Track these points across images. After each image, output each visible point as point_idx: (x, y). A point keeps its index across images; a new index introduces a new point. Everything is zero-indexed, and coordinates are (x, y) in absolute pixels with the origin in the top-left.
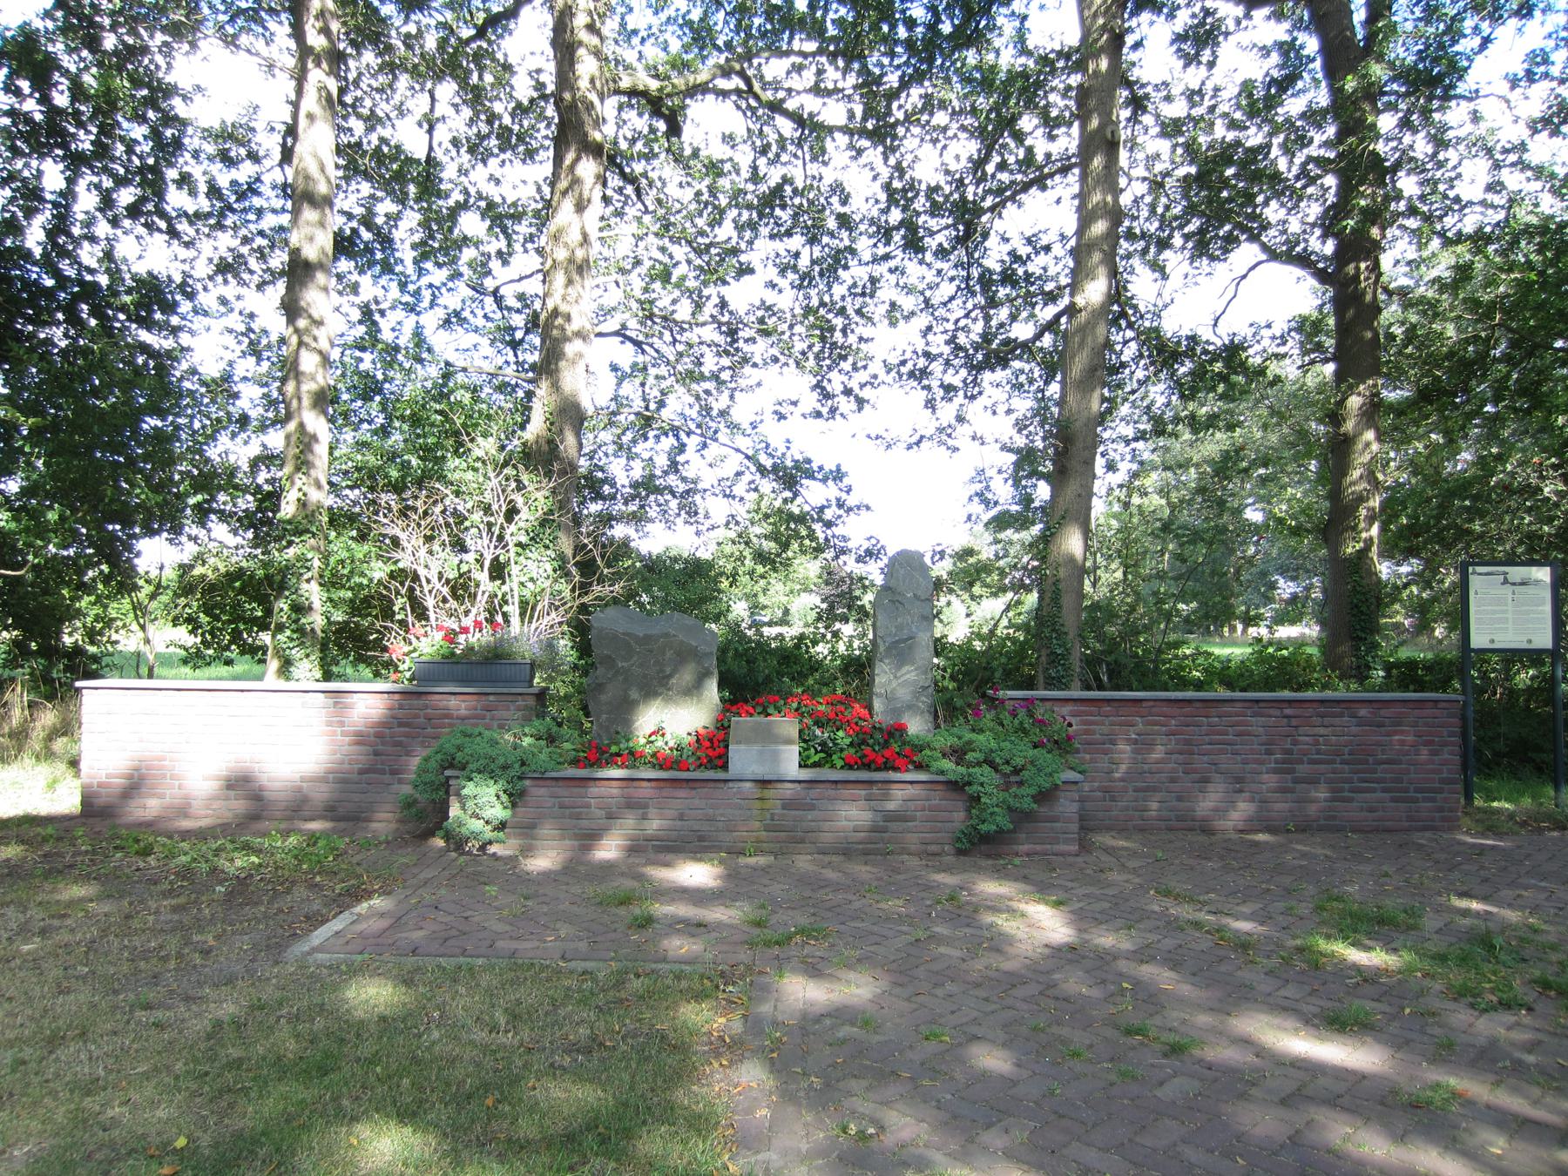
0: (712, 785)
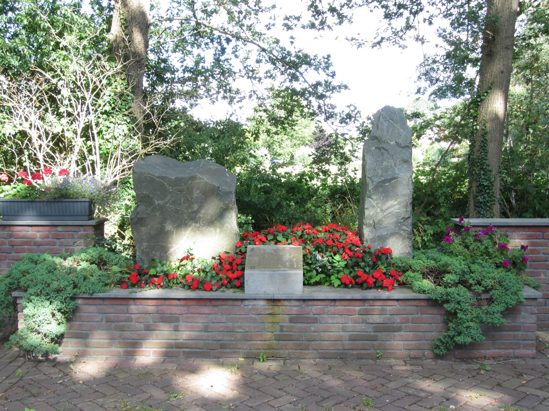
0: (230, 303)
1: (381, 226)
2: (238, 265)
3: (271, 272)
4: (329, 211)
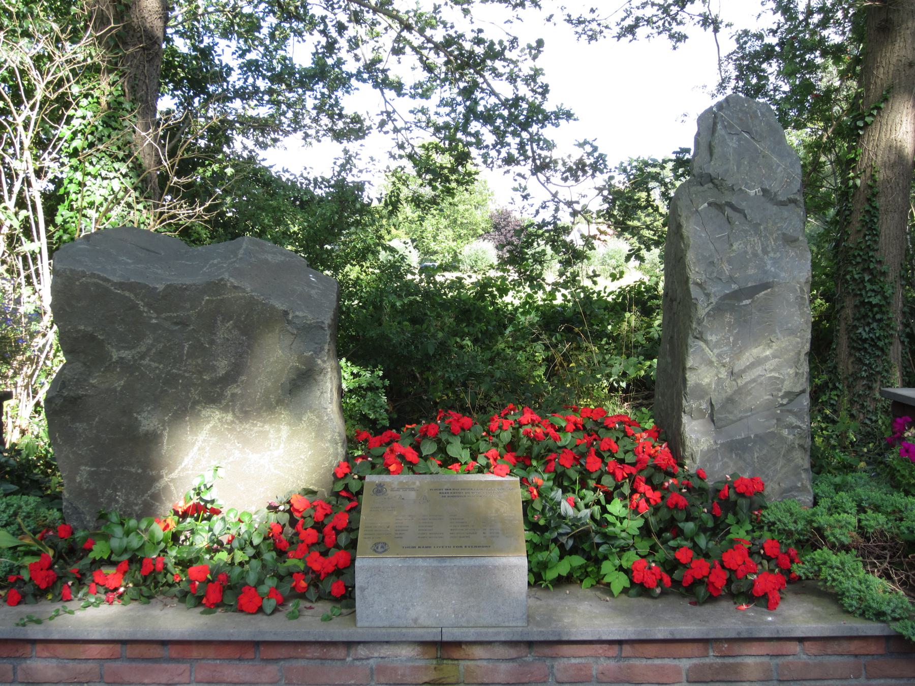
1: (731, 417)
2: (338, 532)
3: (435, 563)
4: (540, 356)
